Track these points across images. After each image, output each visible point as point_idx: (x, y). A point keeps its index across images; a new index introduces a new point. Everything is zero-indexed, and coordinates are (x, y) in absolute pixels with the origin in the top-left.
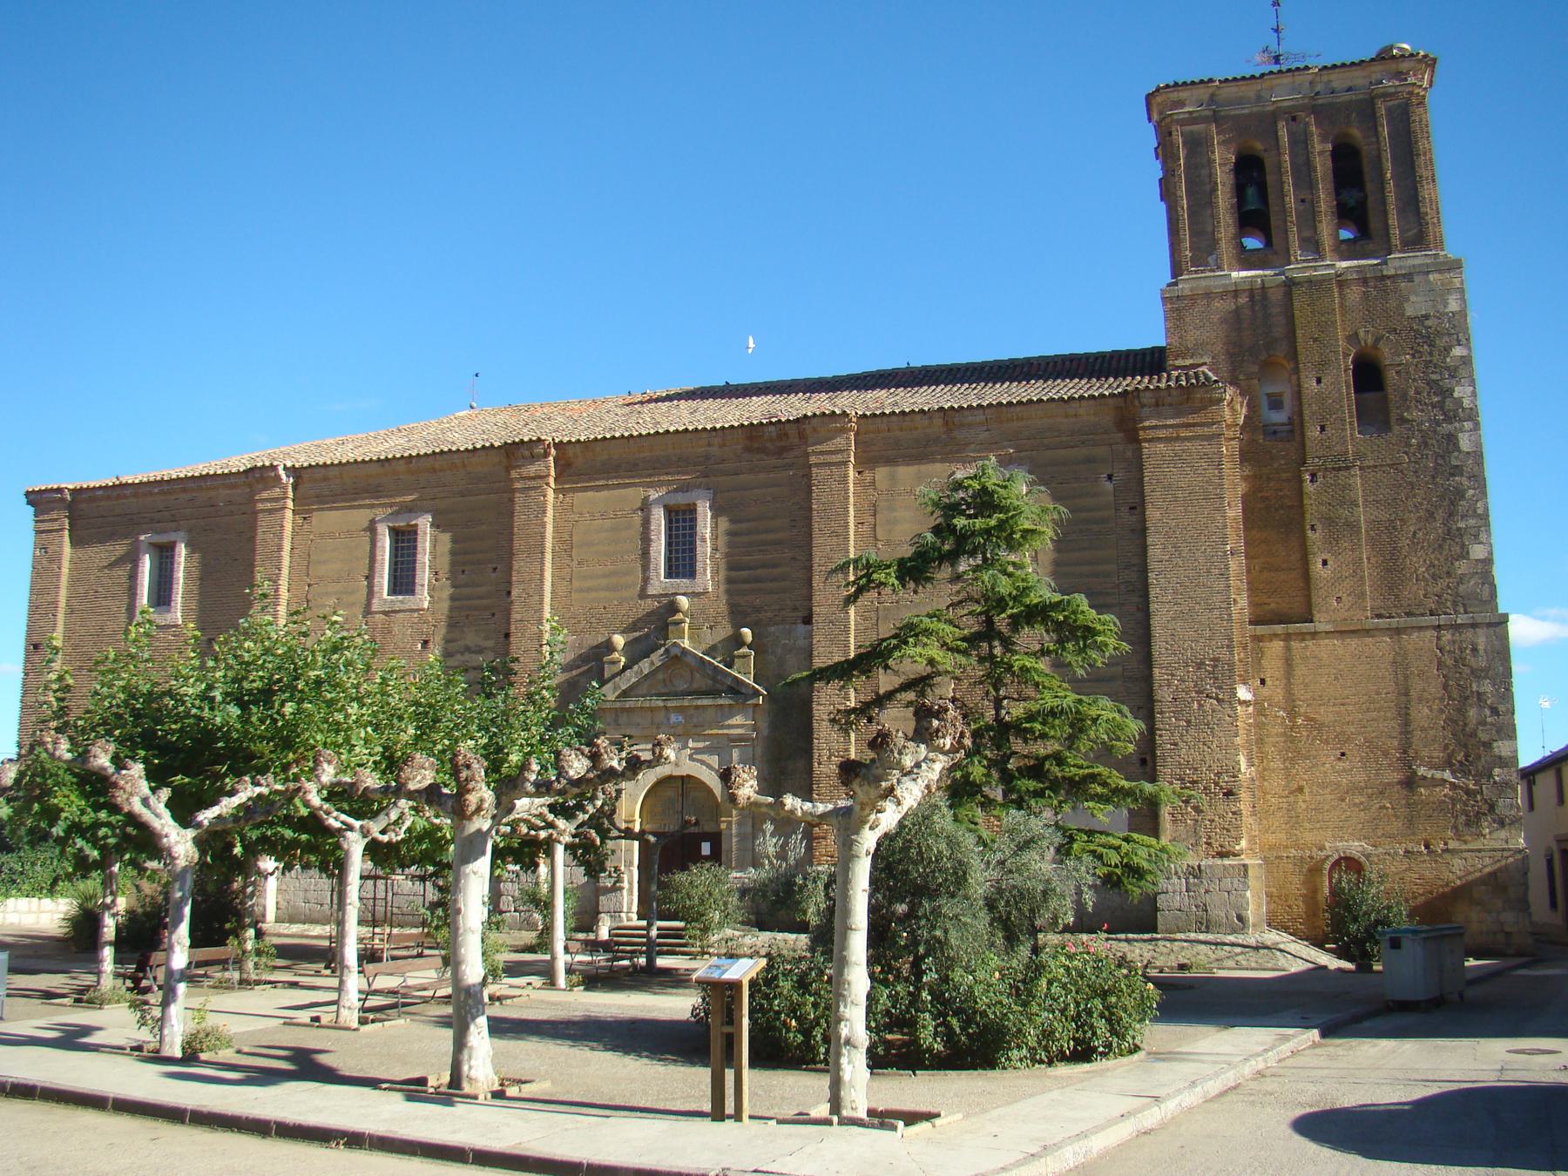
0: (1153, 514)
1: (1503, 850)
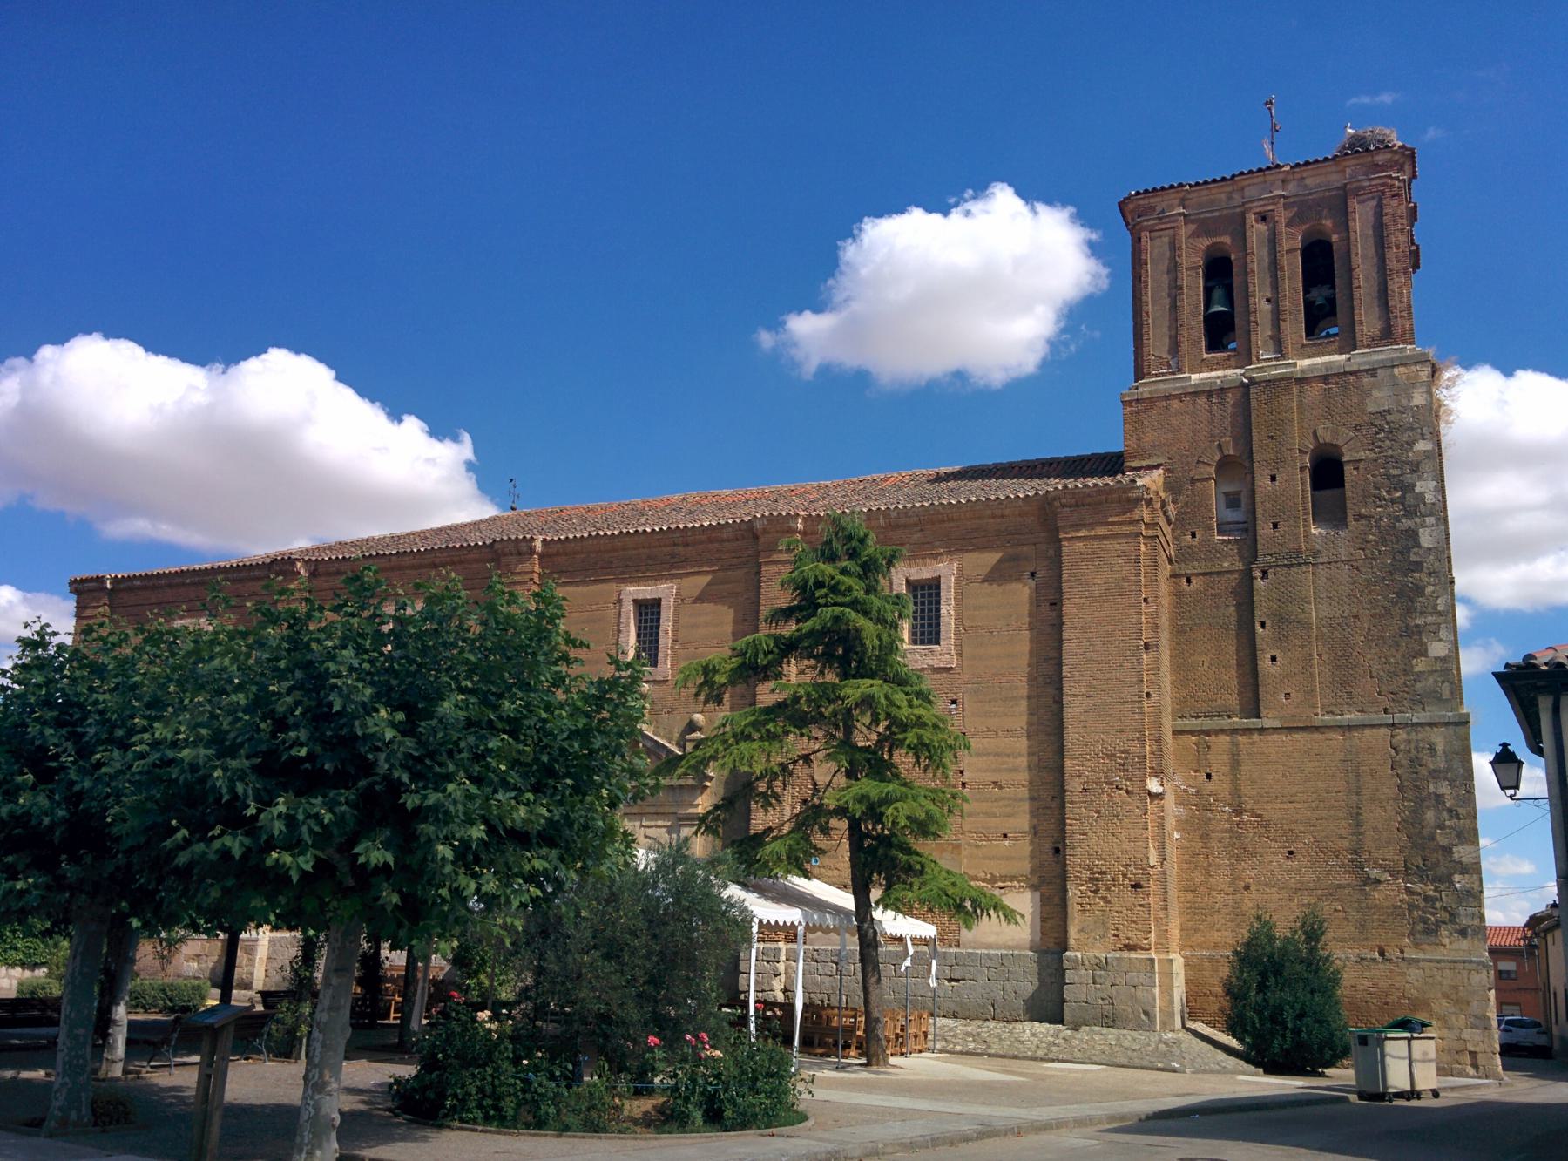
0: (1069, 609)
1: (1464, 962)
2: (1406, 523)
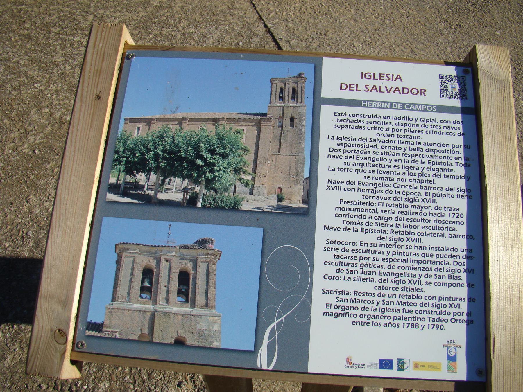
2: (301, 128)
